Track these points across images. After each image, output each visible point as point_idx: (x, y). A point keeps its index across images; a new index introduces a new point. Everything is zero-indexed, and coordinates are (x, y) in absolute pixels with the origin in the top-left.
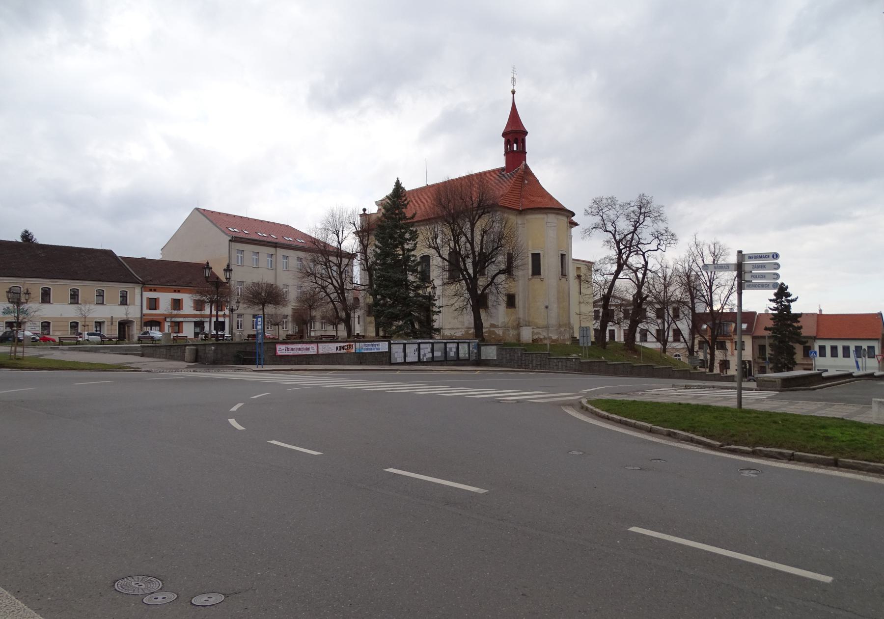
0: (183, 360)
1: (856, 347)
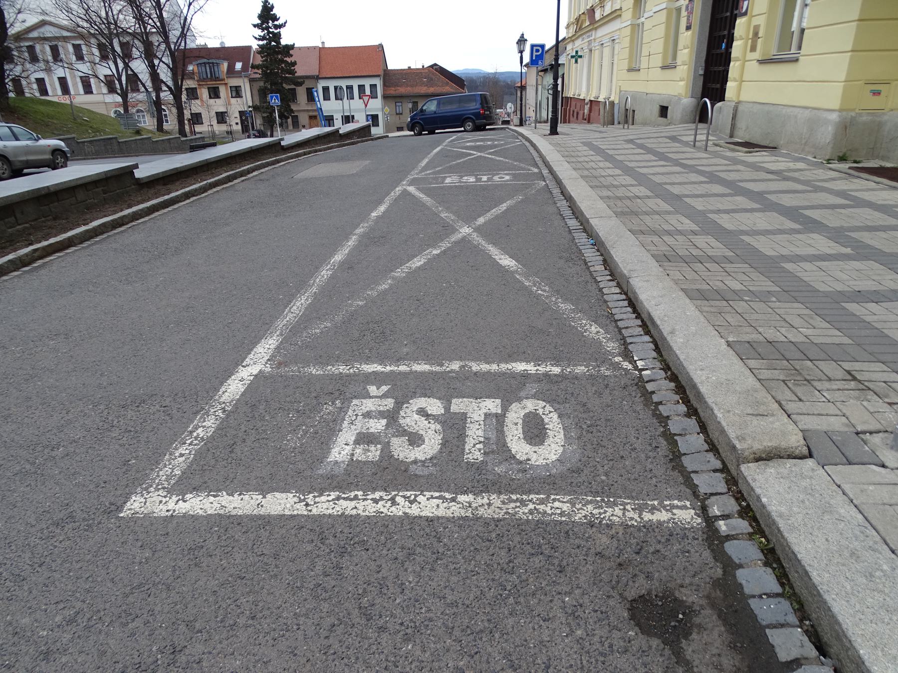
0: (372, 115)
1: (359, 86)
